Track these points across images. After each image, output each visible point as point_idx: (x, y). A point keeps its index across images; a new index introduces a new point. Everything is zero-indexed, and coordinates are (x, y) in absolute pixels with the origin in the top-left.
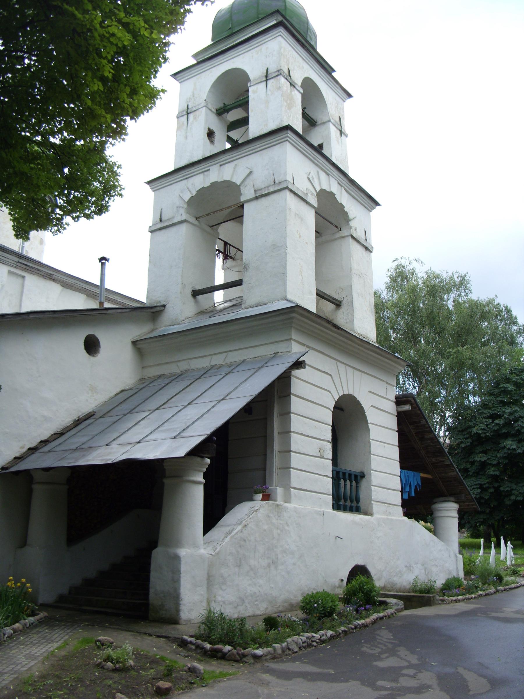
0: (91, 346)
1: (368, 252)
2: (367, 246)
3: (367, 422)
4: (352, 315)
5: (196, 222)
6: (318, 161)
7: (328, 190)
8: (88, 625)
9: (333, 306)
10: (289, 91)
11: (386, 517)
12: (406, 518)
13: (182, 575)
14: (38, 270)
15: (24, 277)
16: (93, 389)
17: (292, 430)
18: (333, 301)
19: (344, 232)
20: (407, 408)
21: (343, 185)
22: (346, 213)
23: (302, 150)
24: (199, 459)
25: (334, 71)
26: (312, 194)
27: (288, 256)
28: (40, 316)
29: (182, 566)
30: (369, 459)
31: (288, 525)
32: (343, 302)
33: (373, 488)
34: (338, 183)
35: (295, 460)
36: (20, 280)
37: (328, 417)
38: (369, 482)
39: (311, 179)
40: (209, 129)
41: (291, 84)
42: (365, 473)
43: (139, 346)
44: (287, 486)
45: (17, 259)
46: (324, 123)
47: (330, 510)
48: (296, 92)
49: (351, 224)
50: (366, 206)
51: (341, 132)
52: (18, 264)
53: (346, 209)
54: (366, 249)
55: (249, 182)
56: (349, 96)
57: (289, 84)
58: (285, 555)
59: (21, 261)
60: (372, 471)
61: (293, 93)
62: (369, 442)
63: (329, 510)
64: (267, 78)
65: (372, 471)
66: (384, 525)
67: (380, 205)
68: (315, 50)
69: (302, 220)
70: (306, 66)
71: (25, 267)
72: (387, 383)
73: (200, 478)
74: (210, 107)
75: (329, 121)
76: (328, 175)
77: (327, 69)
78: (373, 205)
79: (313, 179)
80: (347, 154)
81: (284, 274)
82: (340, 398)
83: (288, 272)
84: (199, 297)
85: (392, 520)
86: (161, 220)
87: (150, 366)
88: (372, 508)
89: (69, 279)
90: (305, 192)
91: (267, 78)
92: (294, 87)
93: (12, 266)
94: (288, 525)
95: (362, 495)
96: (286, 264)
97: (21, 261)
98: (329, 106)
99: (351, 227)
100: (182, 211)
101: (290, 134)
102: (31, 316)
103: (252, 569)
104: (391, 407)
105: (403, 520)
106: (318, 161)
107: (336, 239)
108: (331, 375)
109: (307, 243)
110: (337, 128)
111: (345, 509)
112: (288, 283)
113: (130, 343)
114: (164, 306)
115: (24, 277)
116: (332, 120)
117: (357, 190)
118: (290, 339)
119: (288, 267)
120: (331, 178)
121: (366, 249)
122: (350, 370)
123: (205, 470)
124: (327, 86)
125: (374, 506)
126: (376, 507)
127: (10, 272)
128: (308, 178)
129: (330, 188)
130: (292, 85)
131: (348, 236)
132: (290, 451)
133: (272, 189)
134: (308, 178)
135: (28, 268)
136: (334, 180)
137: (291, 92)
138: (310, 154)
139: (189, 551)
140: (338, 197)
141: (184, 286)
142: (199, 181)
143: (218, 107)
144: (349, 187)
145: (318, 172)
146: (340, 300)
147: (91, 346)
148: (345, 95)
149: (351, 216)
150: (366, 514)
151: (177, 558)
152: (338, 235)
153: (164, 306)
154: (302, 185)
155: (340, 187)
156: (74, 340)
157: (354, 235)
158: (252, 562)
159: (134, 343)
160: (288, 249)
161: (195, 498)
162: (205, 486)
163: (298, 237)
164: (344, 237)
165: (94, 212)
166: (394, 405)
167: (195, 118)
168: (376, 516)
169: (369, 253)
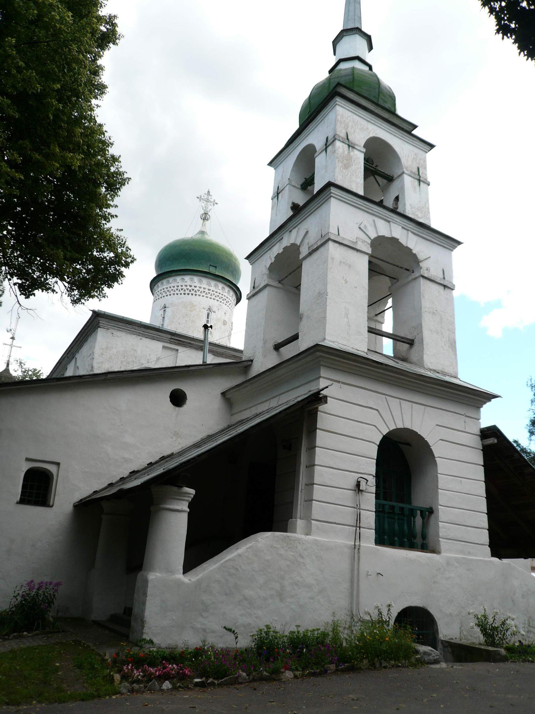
0: (178, 399)
1: (447, 291)
2: (445, 284)
3: (434, 457)
4: (423, 352)
5: (280, 285)
6: (373, 211)
7: (388, 235)
8: (37, 635)
9: (407, 346)
10: (346, 153)
11: (461, 556)
12: (496, 560)
13: (148, 598)
14: (190, 343)
15: (177, 350)
16: (176, 434)
17: (316, 463)
18: (402, 340)
19: (416, 274)
20: (493, 441)
21: (410, 229)
22: (415, 256)
23: (351, 203)
24: (175, 489)
25: (415, 127)
26: (364, 242)
27: (328, 301)
28: (118, 375)
29: (149, 589)
30: (437, 493)
31: (303, 557)
32: (416, 340)
33: (441, 524)
34: (403, 227)
35: (318, 492)
36: (174, 353)
37: (373, 451)
38: (437, 517)
39: (362, 228)
40: (293, 203)
41: (349, 146)
42: (434, 509)
43: (227, 397)
44: (308, 518)
45: (170, 336)
46: (400, 176)
47: (373, 545)
48: (356, 152)
49: (421, 264)
50: (445, 245)
51: (419, 180)
52: (171, 340)
53: (414, 252)
54: (445, 286)
55: (306, 241)
56: (432, 146)
57: (347, 146)
58: (296, 588)
59: (173, 337)
60: (439, 507)
61: (352, 154)
62: (437, 476)
63: (372, 546)
64: (327, 146)
65: (439, 507)
66: (456, 564)
67: (459, 243)
68: (393, 113)
69: (350, 266)
70: (371, 127)
71: (177, 342)
72: (466, 416)
73: (184, 506)
74: (293, 183)
75: (403, 173)
76: (389, 222)
77: (407, 128)
78: (455, 244)
79: (365, 227)
80: (428, 201)
81: (325, 318)
82: (390, 433)
83: (327, 315)
84: (282, 350)
85: (472, 560)
86: (254, 288)
87: (237, 413)
88: (440, 545)
89: (218, 348)
90: (355, 241)
91: (327, 146)
92: (353, 147)
93: (167, 342)
94: (303, 557)
95: (431, 531)
96: (326, 308)
97: (173, 337)
98: (403, 160)
99: (421, 268)
100: (265, 277)
101: (333, 190)
102: (109, 376)
103: (246, 599)
104: (477, 442)
105: (491, 561)
106: (373, 211)
107: (410, 281)
108: (377, 410)
109: (356, 287)
110: (415, 178)
111: (392, 544)
112: (328, 326)
113: (220, 395)
114: (252, 361)
115: (177, 350)
116: (406, 172)
117: (428, 232)
118: (320, 377)
119: (327, 312)
120: (392, 224)
121: (445, 286)
122: (405, 405)
123: (190, 499)
124: (402, 141)
125: (442, 544)
126: (444, 544)
127: (164, 347)
128: (360, 228)
129: (391, 234)
130: (351, 146)
131: (419, 277)
132: (314, 484)
133: (319, 243)
134: (360, 228)
135: (180, 343)
136: (396, 225)
137: (349, 153)
138: (362, 206)
139: (159, 575)
140: (403, 241)
141: (265, 342)
142: (277, 249)
143: (301, 183)
144: (418, 230)
145: (374, 221)
146: (413, 338)
147: (178, 399)
148: (428, 148)
149: (421, 257)
150: (433, 551)
151: (146, 581)
152: (410, 278)
153: (252, 361)
154: (350, 234)
155: (405, 231)
156: (162, 393)
157: (426, 275)
158: (249, 593)
159: (223, 394)
160: (329, 294)
161: (174, 526)
162: (189, 514)
163: (344, 282)
164: (416, 279)
165: (41, 278)
166: (479, 438)
167: (282, 197)
168: (443, 554)
169: (449, 290)
